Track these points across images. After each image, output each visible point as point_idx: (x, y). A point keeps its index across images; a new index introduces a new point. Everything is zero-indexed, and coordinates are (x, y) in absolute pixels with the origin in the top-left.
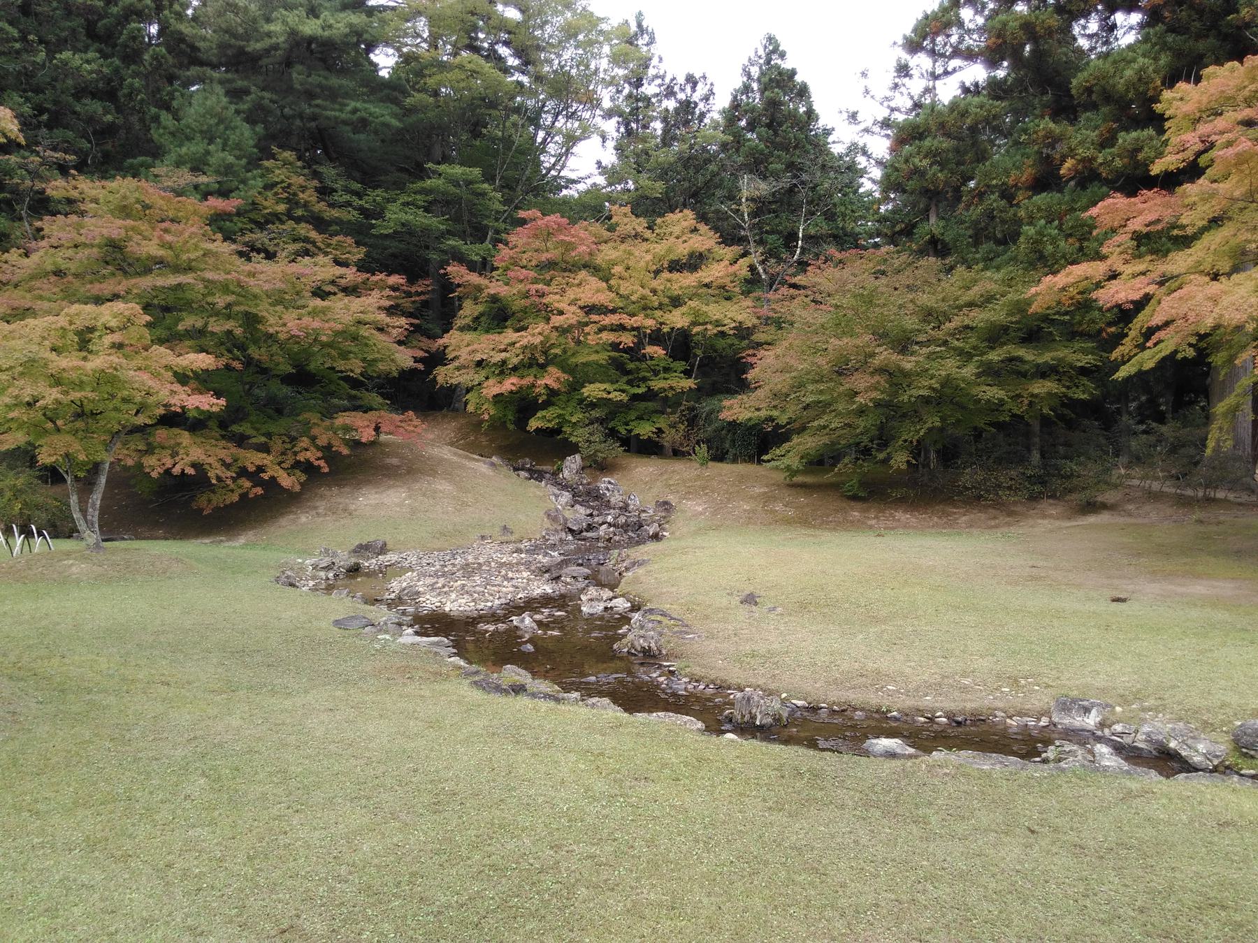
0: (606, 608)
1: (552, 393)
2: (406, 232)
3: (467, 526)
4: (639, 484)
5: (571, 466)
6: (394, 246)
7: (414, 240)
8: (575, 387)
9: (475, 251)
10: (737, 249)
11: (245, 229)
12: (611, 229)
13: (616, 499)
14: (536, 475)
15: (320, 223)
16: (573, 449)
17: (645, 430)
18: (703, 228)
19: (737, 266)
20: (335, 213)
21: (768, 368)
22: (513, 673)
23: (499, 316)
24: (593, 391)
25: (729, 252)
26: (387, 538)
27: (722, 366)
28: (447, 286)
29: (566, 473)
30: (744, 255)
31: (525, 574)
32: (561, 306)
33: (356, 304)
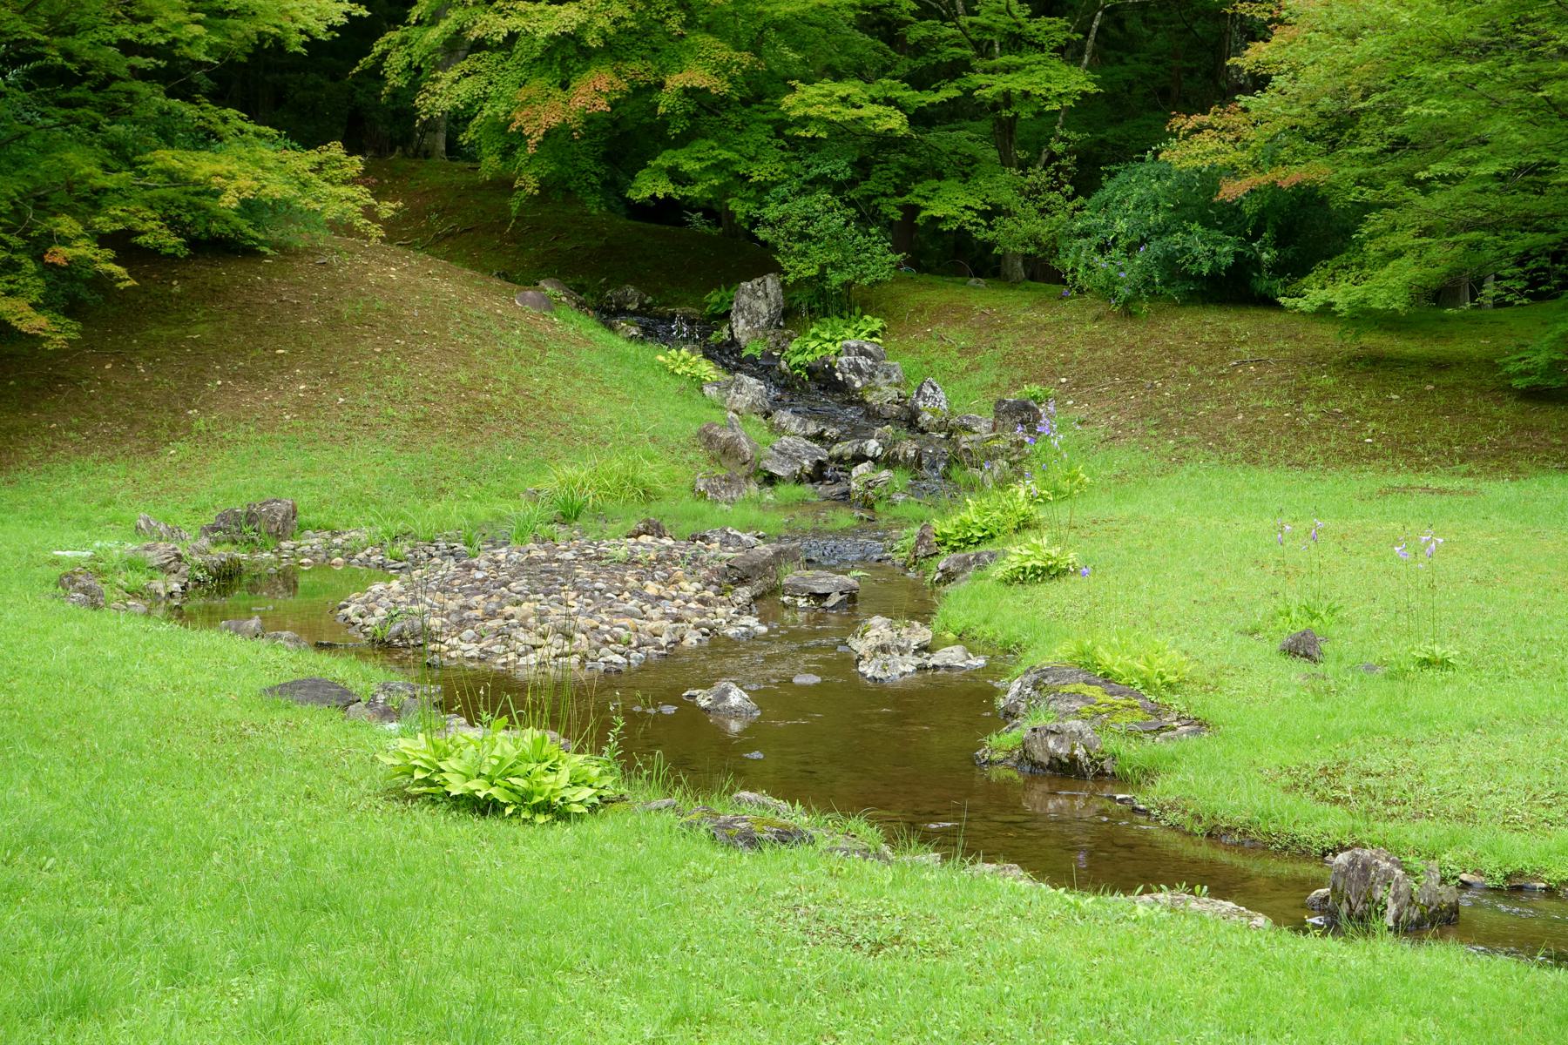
0: (921, 668)
4: (940, 360)
5: (752, 308)
14: (655, 328)
16: (762, 261)
17: (948, 204)
22: (753, 806)
24: (811, 101)
26: (304, 500)
29: (741, 327)
31: (690, 588)
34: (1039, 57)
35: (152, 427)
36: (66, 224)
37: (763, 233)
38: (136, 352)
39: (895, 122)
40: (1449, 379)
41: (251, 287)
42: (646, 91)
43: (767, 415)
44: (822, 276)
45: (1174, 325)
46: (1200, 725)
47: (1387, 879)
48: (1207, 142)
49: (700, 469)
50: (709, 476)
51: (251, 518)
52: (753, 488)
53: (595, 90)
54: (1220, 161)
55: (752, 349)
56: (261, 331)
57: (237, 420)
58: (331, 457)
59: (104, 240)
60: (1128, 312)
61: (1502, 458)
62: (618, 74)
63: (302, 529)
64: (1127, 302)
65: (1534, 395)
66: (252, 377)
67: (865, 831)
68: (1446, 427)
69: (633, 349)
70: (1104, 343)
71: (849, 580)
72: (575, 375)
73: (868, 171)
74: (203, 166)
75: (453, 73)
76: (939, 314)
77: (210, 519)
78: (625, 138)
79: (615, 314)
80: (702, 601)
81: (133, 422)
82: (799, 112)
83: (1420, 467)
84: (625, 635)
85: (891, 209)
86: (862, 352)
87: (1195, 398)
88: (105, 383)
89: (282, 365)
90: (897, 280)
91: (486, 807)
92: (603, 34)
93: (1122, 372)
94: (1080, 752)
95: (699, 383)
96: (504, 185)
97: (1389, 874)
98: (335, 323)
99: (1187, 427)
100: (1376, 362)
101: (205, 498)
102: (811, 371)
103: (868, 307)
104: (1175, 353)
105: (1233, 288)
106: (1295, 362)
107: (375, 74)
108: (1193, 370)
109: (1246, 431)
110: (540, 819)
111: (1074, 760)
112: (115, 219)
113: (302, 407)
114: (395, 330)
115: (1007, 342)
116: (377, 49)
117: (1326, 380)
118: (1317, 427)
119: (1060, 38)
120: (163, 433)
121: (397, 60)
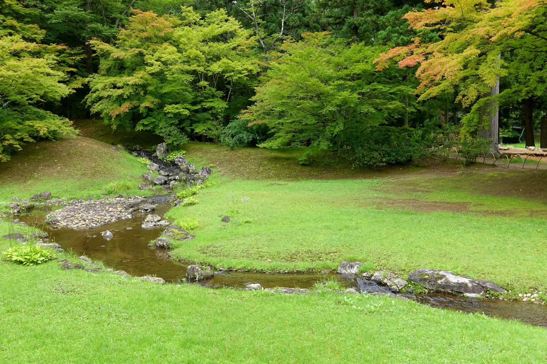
1: (149, 109)
2: (68, 20)
3: (100, 185)
4: (194, 159)
5: (160, 150)
6: (64, 29)
7: (74, 24)
8: (161, 106)
9: (106, 30)
10: (250, 31)
11: (35, 37)
12: (183, 18)
13: (184, 166)
15: (19, 17)
16: (160, 140)
17: (199, 129)
18: (232, 19)
19: (250, 40)
20: (28, 11)
21: (266, 93)
23: (121, 67)
25: (246, 32)
27: (238, 93)
28: (89, 50)
29: (158, 153)
30: (255, 34)
32: (153, 61)
33: (36, 61)
34: (217, 99)
35: (26, 177)
36: (8, 136)
37: (161, 135)
38: (25, 161)
39: (187, 112)
40: (289, 162)
41: (53, 147)
42: (137, 107)
43: (159, 171)
44: (173, 143)
45: (241, 152)
46: (193, 237)
47: (197, 271)
48: (246, 115)
49: (141, 182)
50: (141, 184)
51: (40, 196)
52: (151, 187)
53: (125, 107)
54: (248, 118)
55: (160, 157)
56: (53, 156)
57: (44, 175)
58: (62, 182)
59: (16, 140)
60: (232, 149)
61: (296, 177)
62: (131, 103)
63: (52, 198)
64: (232, 147)
65: (304, 165)
66: (49, 166)
67: (450, 214)
68: (287, 171)
69: (135, 158)
70: (227, 155)
71: (154, 206)
72: (119, 164)
73: (181, 122)
74: (38, 124)
75: (98, 104)
76: (197, 150)
77: (32, 196)
78: (135, 116)
79: (133, 151)
80: (121, 212)
81: (22, 176)
82: (167, 111)
83: (280, 179)
84: (97, 220)
85: (188, 129)
86: (180, 158)
87: (240, 166)
88: (18, 168)
89: (55, 163)
90: (189, 143)
91: (21, 263)
92: (127, 95)
93: (229, 161)
94: (165, 244)
95: (146, 165)
96: (110, 125)
97: (198, 269)
98: (69, 155)
99: (237, 172)
100: (276, 159)
101: (33, 192)
102: (171, 162)
103: (184, 149)
104: (239, 157)
105: (253, 144)
106: (261, 159)
107: (85, 103)
108: (242, 161)
109: (248, 173)
110: (31, 264)
111: (164, 245)
112: (19, 136)
113: (58, 172)
114: (81, 156)
115: (209, 155)
116: (86, 98)
117: (266, 162)
118: (262, 172)
119: (221, 95)
120: (28, 178)
121: (89, 100)
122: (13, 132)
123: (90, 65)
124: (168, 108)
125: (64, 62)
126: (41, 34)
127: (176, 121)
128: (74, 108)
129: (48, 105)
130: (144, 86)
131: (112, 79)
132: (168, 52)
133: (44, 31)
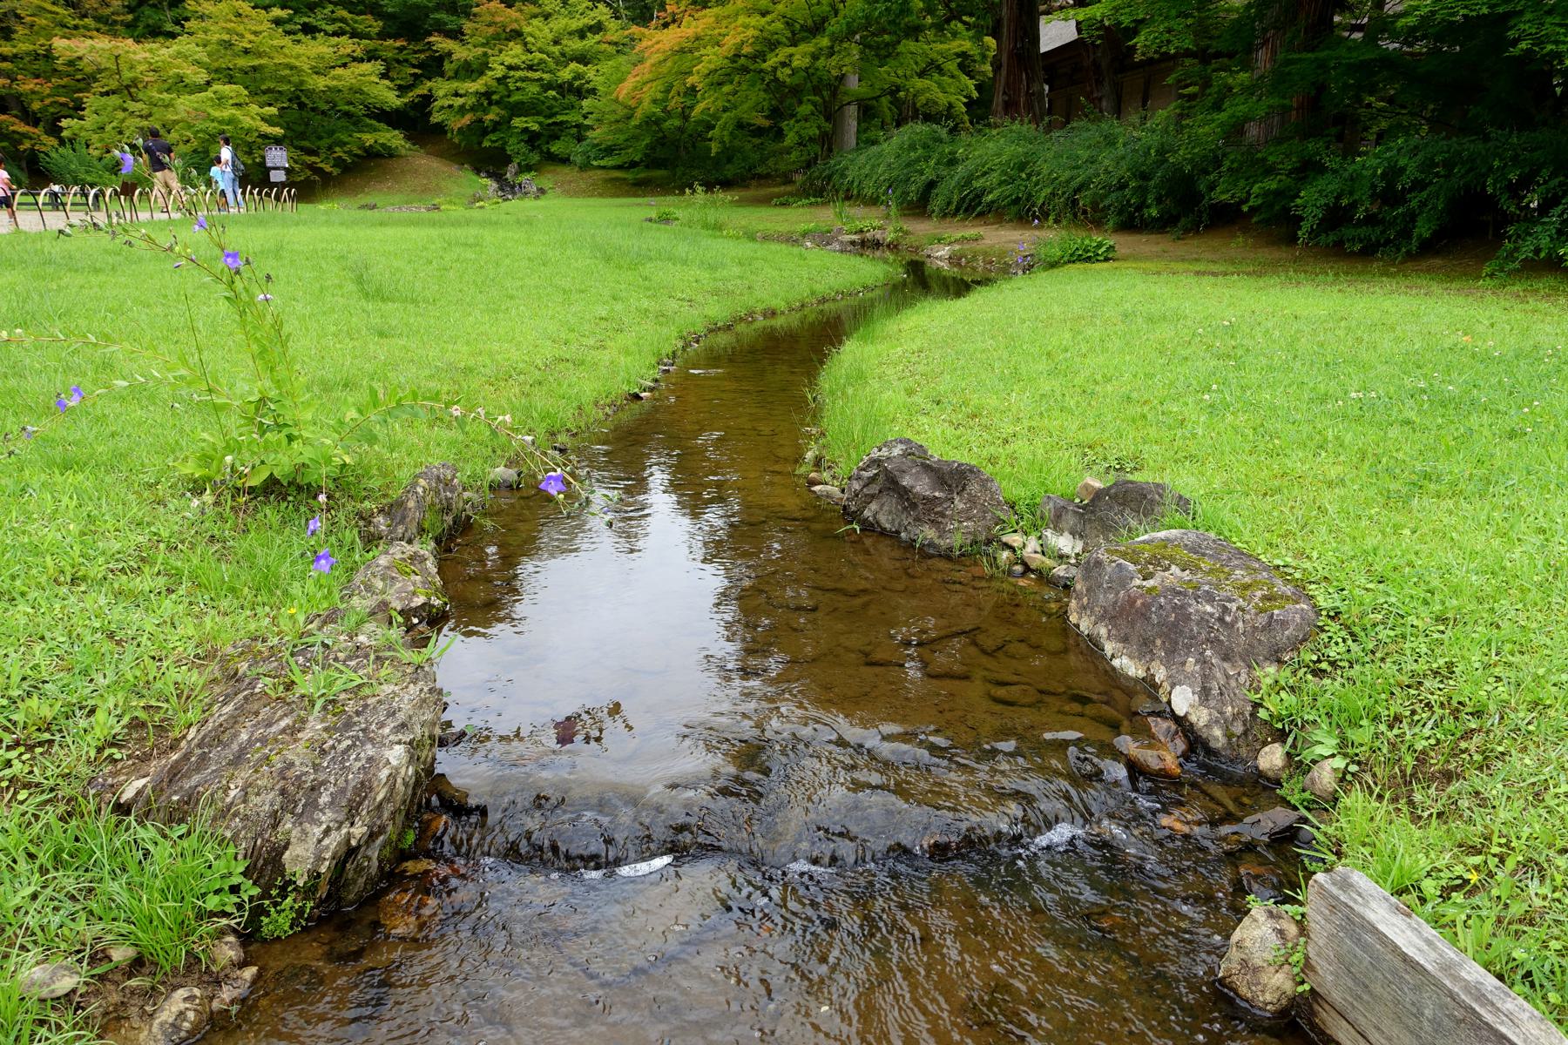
42: (480, 121)
53: (467, 119)
73: (532, 139)
74: (365, 136)
122: (343, 144)
123: (434, 66)
124: (518, 122)
125: (406, 61)
126: (377, 26)
127: (525, 137)
128: (415, 121)
129: (391, 118)
130: (487, 95)
131: (455, 85)
132: (514, 53)
133: (381, 23)
